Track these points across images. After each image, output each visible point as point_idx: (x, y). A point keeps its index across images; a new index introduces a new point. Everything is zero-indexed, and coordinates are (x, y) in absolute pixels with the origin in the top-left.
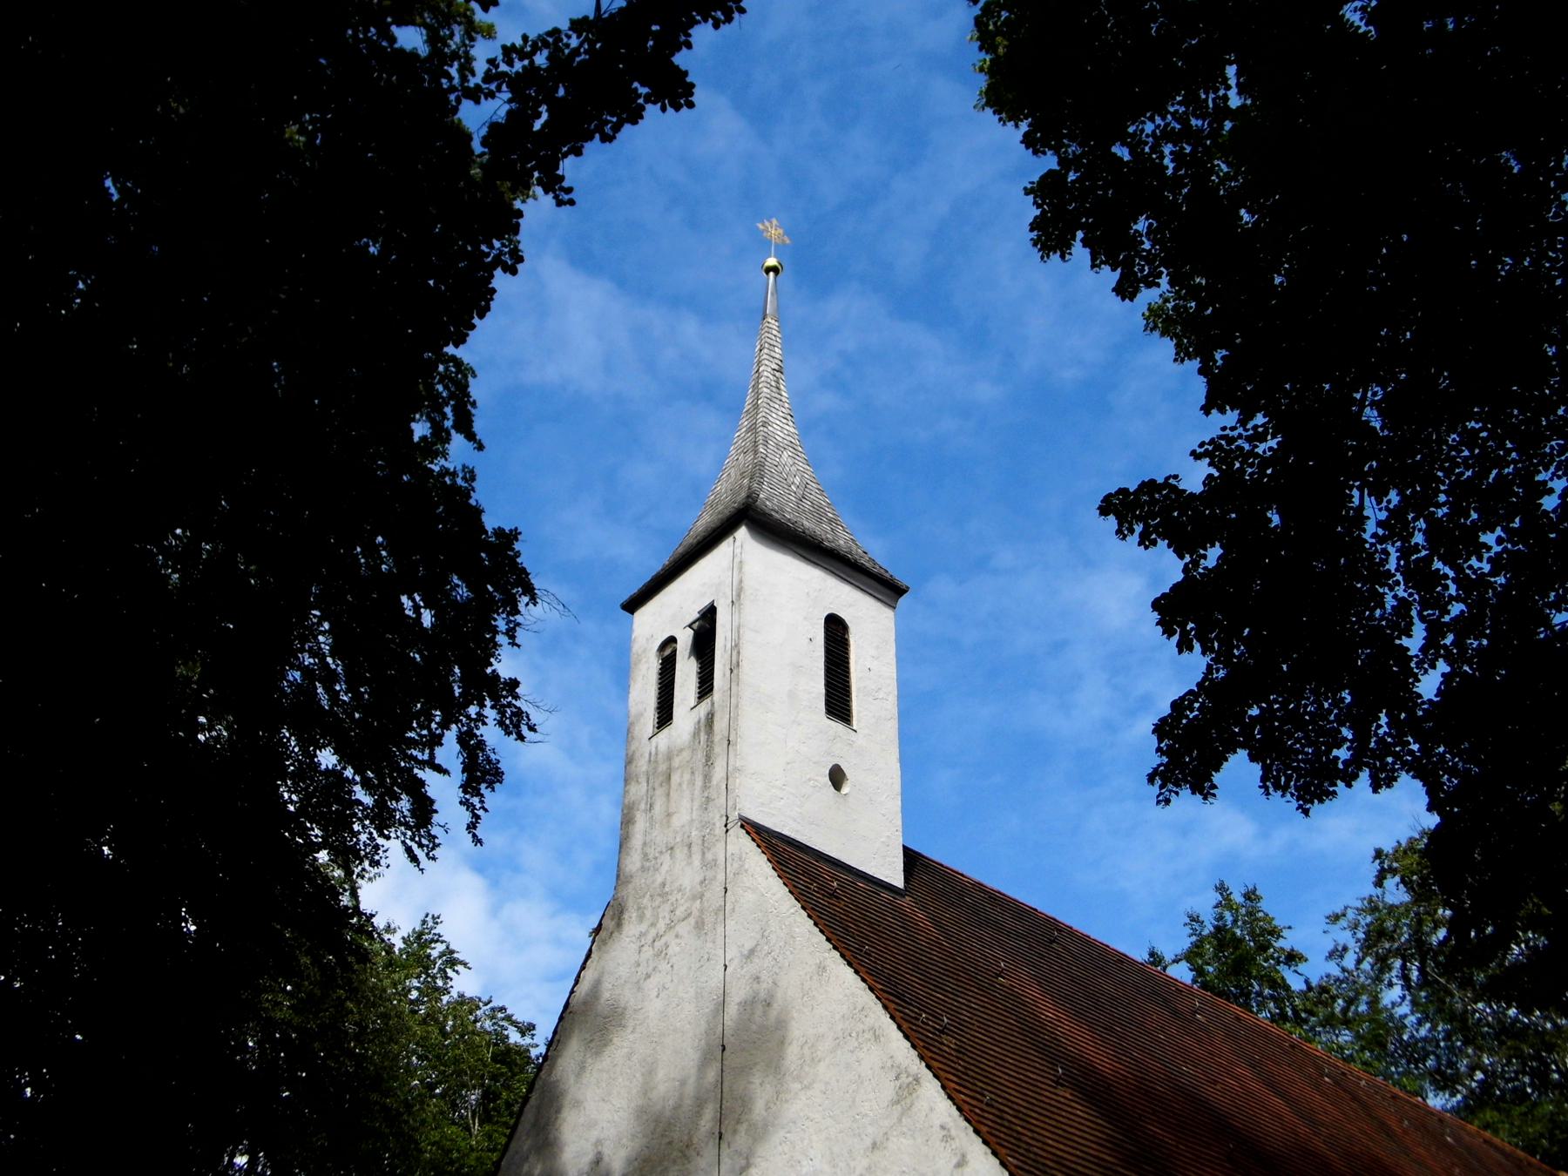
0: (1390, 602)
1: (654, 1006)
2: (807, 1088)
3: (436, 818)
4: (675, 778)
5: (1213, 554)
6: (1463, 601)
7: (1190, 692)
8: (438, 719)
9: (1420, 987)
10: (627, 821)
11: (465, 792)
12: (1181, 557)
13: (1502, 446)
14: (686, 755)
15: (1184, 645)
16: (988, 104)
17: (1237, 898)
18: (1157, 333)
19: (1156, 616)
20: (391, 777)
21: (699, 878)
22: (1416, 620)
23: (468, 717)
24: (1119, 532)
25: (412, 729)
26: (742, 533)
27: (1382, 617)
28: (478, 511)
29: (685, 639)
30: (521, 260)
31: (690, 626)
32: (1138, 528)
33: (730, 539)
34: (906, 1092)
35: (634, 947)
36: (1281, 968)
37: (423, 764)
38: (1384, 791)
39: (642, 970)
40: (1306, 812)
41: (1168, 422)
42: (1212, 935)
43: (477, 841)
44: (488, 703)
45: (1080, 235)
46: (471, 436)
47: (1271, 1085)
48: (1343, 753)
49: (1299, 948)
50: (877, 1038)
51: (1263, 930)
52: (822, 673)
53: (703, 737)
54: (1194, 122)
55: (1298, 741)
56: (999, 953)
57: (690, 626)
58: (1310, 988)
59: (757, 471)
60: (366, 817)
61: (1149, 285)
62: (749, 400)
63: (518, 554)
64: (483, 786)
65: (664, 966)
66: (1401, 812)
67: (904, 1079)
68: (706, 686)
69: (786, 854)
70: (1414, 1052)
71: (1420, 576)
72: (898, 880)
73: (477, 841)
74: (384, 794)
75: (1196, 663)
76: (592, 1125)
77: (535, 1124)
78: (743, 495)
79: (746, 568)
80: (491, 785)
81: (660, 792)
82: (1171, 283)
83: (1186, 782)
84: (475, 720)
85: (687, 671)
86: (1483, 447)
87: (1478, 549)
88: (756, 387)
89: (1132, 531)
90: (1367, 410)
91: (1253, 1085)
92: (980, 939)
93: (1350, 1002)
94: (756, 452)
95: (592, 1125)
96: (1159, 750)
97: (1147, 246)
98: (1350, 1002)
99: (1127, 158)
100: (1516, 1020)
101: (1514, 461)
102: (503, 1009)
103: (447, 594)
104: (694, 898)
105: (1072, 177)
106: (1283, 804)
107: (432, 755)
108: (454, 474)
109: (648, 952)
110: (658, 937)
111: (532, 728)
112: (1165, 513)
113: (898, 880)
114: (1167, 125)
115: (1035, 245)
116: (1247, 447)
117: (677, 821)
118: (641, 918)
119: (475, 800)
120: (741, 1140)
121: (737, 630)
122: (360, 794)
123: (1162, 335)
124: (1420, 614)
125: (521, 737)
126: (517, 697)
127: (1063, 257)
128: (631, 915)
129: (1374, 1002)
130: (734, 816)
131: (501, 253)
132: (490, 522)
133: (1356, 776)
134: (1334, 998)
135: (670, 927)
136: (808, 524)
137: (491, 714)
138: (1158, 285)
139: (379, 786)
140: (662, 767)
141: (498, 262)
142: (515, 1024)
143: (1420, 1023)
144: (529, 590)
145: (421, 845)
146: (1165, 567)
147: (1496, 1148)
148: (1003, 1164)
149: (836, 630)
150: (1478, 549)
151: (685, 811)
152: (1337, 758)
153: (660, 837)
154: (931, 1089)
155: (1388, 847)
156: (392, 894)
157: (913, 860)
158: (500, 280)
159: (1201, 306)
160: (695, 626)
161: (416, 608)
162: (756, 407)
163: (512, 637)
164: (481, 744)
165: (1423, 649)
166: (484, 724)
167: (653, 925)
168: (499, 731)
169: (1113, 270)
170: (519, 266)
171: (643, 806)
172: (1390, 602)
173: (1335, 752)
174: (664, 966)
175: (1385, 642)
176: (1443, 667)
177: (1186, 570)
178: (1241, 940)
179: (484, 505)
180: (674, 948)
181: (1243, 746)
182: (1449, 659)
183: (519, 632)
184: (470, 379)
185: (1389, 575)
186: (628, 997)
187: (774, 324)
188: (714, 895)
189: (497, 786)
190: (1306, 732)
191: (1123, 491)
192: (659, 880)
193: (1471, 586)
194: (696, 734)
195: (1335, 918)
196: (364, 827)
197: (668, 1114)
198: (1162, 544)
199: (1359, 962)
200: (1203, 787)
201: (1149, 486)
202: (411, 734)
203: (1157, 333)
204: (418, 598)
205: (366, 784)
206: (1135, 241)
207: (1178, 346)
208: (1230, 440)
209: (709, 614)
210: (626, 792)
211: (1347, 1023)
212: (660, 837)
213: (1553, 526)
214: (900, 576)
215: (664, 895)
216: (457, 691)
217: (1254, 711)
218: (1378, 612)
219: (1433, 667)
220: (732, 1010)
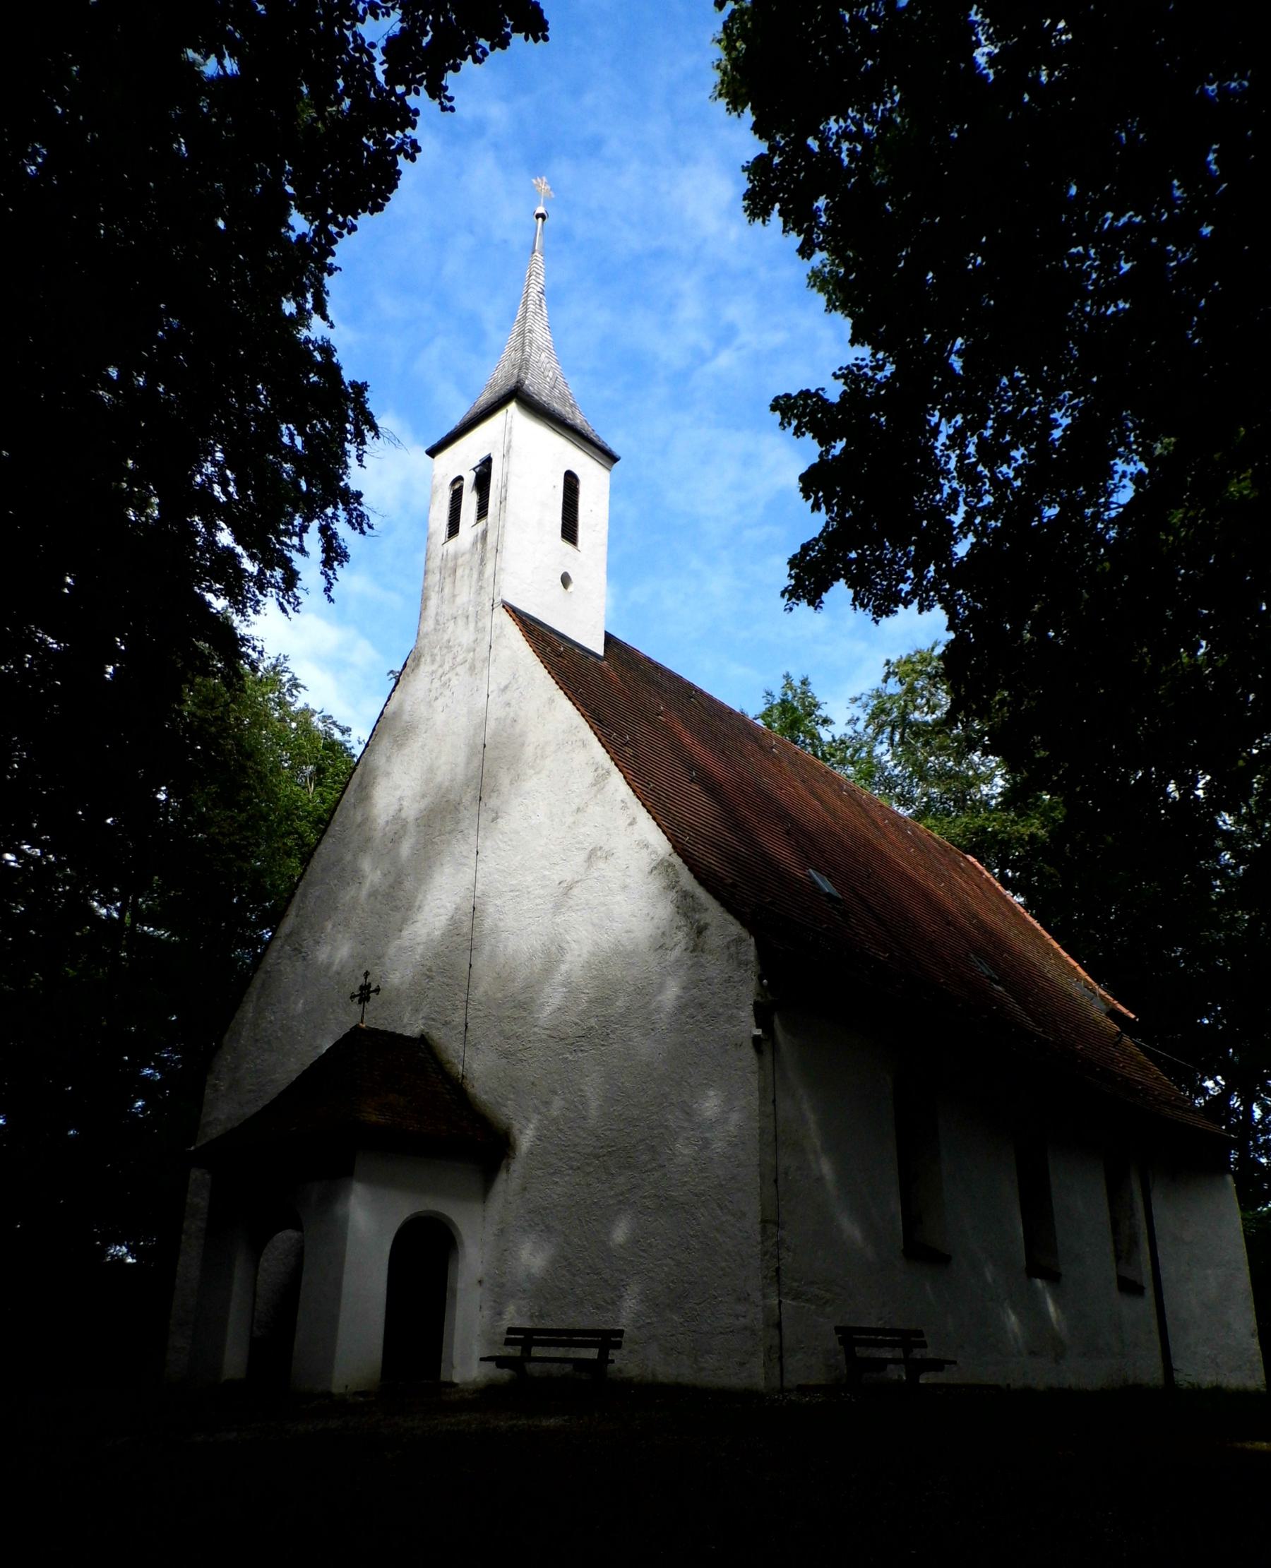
0: (947, 490)
1: (440, 718)
2: (538, 773)
3: (299, 584)
5: (840, 445)
6: (992, 495)
7: (814, 539)
9: (899, 745)
10: (425, 599)
11: (324, 566)
13: (1034, 392)
15: (816, 507)
16: (727, 95)
17: (796, 683)
18: (815, 290)
21: (472, 638)
22: (961, 503)
24: (781, 424)
26: (513, 407)
27: (941, 500)
29: (469, 479)
30: (418, 149)
32: (794, 423)
34: (600, 780)
35: (428, 680)
36: (818, 727)
38: (925, 613)
39: (433, 694)
40: (877, 622)
41: (823, 350)
42: (780, 704)
43: (331, 600)
44: (340, 506)
45: (777, 206)
47: (813, 793)
48: (905, 587)
49: (831, 717)
50: (584, 745)
51: (810, 704)
53: (479, 546)
54: (866, 126)
55: (878, 576)
56: (659, 701)
58: (834, 741)
59: (524, 364)
62: (520, 312)
63: (366, 402)
65: (448, 693)
66: (923, 629)
67: (600, 771)
68: (482, 511)
69: (533, 629)
70: (889, 783)
71: (967, 474)
72: (600, 651)
73: (331, 600)
75: (822, 518)
76: (397, 788)
77: (360, 784)
78: (514, 380)
79: (514, 432)
81: (448, 580)
85: (470, 500)
86: (1022, 391)
87: (1009, 460)
88: (525, 303)
89: (790, 424)
90: (953, 356)
91: (803, 792)
92: (649, 692)
93: (856, 751)
95: (397, 788)
96: (790, 575)
97: (823, 219)
98: (856, 751)
99: (817, 150)
100: (951, 769)
101: (1040, 403)
102: (330, 717)
104: (469, 651)
105: (777, 160)
106: (865, 616)
109: (437, 684)
110: (444, 674)
111: (370, 527)
112: (812, 414)
113: (600, 651)
114: (847, 127)
116: (870, 373)
117: (459, 601)
118: (433, 661)
119: (330, 573)
120: (493, 802)
123: (819, 290)
124: (965, 500)
125: (363, 532)
126: (360, 504)
127: (764, 222)
128: (426, 659)
129: (870, 753)
130: (498, 600)
131: (403, 143)
133: (911, 602)
134: (847, 748)
135: (452, 668)
136: (557, 406)
137: (342, 514)
140: (450, 564)
141: (400, 149)
142: (337, 726)
143: (895, 766)
144: (374, 427)
145: (289, 602)
146: (807, 451)
147: (934, 839)
148: (659, 825)
149: (571, 482)
150: (1009, 460)
151: (465, 595)
152: (901, 590)
153: (447, 610)
154: (617, 779)
155: (894, 659)
156: (268, 629)
157: (609, 639)
159: (847, 273)
162: (525, 318)
163: (360, 461)
164: (335, 535)
165: (961, 526)
167: (441, 666)
170: (417, 155)
172: (947, 490)
173: (901, 586)
174: (448, 693)
175: (939, 515)
176: (971, 538)
177: (821, 456)
178: (796, 709)
180: (454, 682)
181: (844, 577)
182: (976, 534)
185: (949, 472)
186: (423, 710)
188: (482, 650)
190: (884, 571)
191: (788, 396)
192: (446, 637)
193: (1000, 485)
194: (474, 544)
195: (855, 700)
197: (447, 784)
198: (809, 435)
199: (867, 727)
200: (815, 601)
201: (805, 394)
203: (815, 290)
205: (252, 557)
206: (815, 215)
207: (829, 300)
208: (860, 368)
209: (487, 462)
211: (853, 763)
212: (447, 610)
213: (1057, 451)
215: (449, 648)
217: (853, 555)
218: (938, 497)
219: (965, 537)
220: (492, 724)
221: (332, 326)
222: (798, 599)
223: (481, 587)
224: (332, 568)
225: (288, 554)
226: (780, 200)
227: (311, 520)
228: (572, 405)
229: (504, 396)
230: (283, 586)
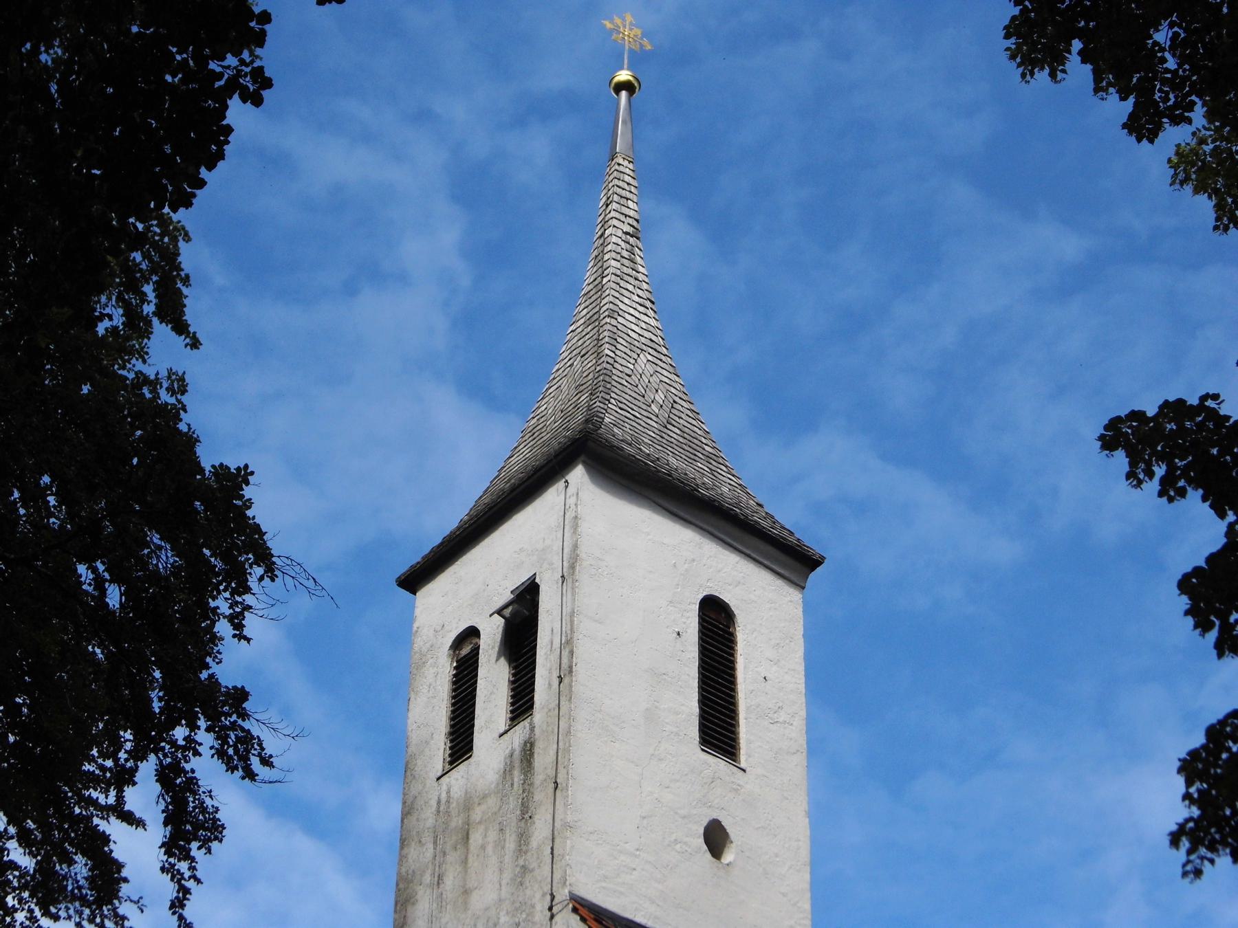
3: (125, 889)
4: (476, 838)
8: (128, 746)
11: (169, 853)
12: (1222, 515)
14: (492, 802)
18: (1188, 188)
19: (1184, 602)
20: (61, 829)
23: (173, 743)
24: (1131, 475)
25: (92, 760)
26: (578, 475)
28: (190, 441)
29: (492, 631)
30: (268, 83)
31: (499, 612)
32: (1160, 471)
33: (561, 484)
37: (106, 811)
44: (202, 723)
45: (1077, 45)
46: (181, 327)
52: (695, 684)
53: (517, 776)
57: (499, 612)
59: (600, 383)
60: (22, 888)
61: (1177, 121)
62: (589, 276)
63: (248, 504)
64: (194, 845)
68: (522, 701)
74: (50, 850)
78: (580, 417)
79: (584, 527)
80: (205, 845)
81: (452, 857)
82: (1210, 116)
83: (1225, 844)
84: (184, 748)
85: (494, 678)
89: (1150, 474)
94: (599, 355)
96: (1187, 796)
97: (1171, 64)
103: (143, 563)
107: (120, 798)
108: (154, 384)
111: (266, 762)
115: (1013, 57)
117: (478, 901)
119: (183, 866)
121: (570, 620)
122: (17, 854)
123: (1196, 191)
125: (250, 775)
126: (244, 715)
127: (1053, 75)
130: (562, 894)
131: (239, 73)
132: (208, 458)
137: (206, 739)
138: (1189, 121)
139: (42, 842)
140: (457, 822)
141: (234, 86)
144: (264, 557)
149: (716, 620)
158: (237, 113)
160: (507, 612)
161: (99, 583)
162: (600, 288)
164: (192, 784)
166: (197, 753)
168: (219, 765)
169: (1123, 99)
170: (266, 94)
171: (427, 878)
179: (199, 432)
183: (250, 620)
184: (181, 244)
187: (627, 167)
189: (215, 845)
194: (507, 772)
196: (20, 901)
198: (1194, 495)
201: (1174, 409)
202: (87, 767)
203: (1188, 188)
204: (101, 567)
205: (25, 839)
206: (1152, 58)
207: (1219, 207)
209: (528, 595)
210: (402, 858)
214: (811, 537)
216: (156, 706)
221: (195, 344)
222: (1212, 848)
223: (525, 869)
224: (187, 856)
225: (103, 825)
226: (1080, 34)
227: (144, 758)
228: (708, 456)
229: (558, 454)
230: (90, 895)
